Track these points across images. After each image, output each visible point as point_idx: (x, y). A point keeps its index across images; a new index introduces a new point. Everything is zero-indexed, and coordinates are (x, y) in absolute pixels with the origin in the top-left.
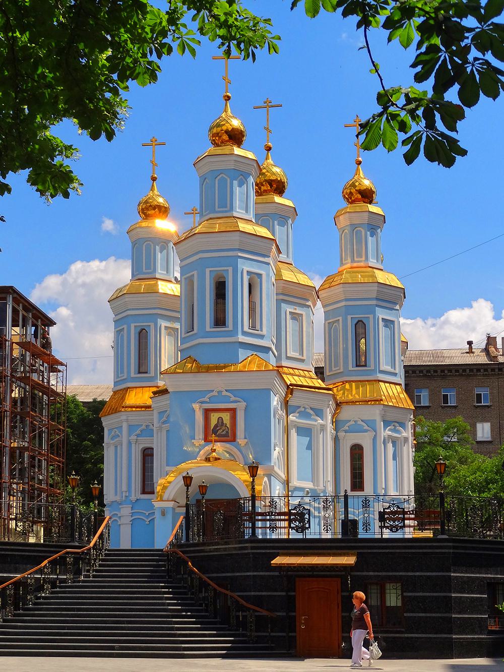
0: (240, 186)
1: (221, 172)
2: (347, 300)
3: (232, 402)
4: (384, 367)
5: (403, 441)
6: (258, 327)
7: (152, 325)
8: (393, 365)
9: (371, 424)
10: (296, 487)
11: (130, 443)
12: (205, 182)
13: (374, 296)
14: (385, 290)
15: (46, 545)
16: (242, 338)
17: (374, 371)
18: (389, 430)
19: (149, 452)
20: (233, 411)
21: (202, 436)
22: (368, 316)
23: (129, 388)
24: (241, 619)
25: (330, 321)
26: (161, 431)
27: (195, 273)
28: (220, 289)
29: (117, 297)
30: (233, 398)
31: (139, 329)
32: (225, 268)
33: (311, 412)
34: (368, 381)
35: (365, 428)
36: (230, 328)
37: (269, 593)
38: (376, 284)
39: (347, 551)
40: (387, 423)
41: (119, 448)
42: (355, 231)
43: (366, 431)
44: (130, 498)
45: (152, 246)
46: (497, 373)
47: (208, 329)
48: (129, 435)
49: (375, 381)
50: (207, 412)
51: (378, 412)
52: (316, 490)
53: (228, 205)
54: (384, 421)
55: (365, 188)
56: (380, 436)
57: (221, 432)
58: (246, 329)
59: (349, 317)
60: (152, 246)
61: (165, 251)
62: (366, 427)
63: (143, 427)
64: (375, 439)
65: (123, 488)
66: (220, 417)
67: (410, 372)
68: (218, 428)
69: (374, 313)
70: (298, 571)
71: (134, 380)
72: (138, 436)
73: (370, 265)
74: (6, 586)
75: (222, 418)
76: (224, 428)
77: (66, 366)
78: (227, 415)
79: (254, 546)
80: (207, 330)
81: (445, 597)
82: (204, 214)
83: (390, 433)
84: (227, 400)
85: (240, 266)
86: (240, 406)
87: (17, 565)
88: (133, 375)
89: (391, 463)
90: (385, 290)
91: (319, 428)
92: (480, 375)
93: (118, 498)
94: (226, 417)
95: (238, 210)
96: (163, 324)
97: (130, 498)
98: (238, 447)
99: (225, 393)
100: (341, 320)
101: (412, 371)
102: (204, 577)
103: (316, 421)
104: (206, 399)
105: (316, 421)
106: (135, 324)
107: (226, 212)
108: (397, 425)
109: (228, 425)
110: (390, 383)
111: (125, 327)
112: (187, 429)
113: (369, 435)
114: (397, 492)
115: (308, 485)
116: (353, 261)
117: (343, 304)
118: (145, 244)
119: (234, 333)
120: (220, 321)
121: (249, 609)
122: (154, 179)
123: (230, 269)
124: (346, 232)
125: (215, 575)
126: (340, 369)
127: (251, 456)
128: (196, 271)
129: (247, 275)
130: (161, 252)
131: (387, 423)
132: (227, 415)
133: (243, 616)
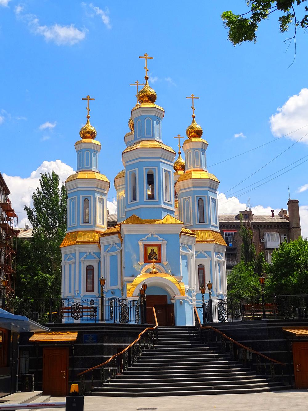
0: (157, 124)
1: (149, 116)
2: (194, 187)
4: (213, 224)
5: (223, 263)
6: (169, 200)
7: (92, 196)
8: (216, 223)
9: (209, 253)
11: (80, 263)
12: (138, 121)
13: (207, 185)
14: (213, 183)
15: (138, 325)
17: (208, 225)
18: (217, 257)
19: (90, 268)
20: (159, 246)
21: (143, 260)
22: (205, 196)
23: (78, 231)
24: (265, 367)
25: (184, 198)
26: (106, 256)
27: (137, 169)
30: (160, 239)
32: (135, 169)
33: (187, 247)
34: (205, 230)
35: (205, 256)
36: (157, 200)
37: (278, 352)
39: (298, 327)
40: (216, 253)
41: (73, 266)
42: (195, 152)
43: (206, 257)
44: (80, 294)
45: (199, 152)
46: (225, 227)
47: (145, 200)
48: (80, 258)
49: (209, 230)
50: (146, 246)
51: (212, 247)
53: (152, 134)
54: (215, 252)
56: (214, 260)
57: (152, 257)
59: (195, 196)
60: (199, 152)
61: (96, 156)
62: (206, 255)
63: (88, 254)
65: (76, 288)
66: (152, 249)
67: (222, 226)
68: (151, 255)
69: (207, 194)
70: (303, 338)
71: (82, 227)
72: (84, 258)
73: (203, 170)
75: (153, 249)
76: (154, 255)
77: (17, 218)
78: (156, 248)
79: (269, 324)
80: (145, 201)
82: (137, 138)
84: (156, 239)
85: (161, 167)
86: (164, 243)
88: (81, 224)
89: (218, 274)
90: (213, 183)
91: (191, 255)
92: (225, 228)
93: (72, 295)
94: (156, 249)
95: (156, 137)
96: (98, 196)
97: (80, 294)
98: (163, 265)
101: (230, 225)
102: (237, 342)
104: (145, 239)
105: (189, 251)
106: (82, 196)
107: (151, 137)
108: (220, 254)
111: (76, 197)
112: (135, 256)
113: (208, 259)
116: (194, 167)
117: (192, 189)
119: (159, 202)
121: (271, 361)
122: (194, 117)
123: (157, 168)
124: (190, 152)
125: (243, 341)
126: (191, 224)
127: (170, 272)
130: (94, 157)
131: (216, 253)
132: (156, 248)
133: (266, 365)
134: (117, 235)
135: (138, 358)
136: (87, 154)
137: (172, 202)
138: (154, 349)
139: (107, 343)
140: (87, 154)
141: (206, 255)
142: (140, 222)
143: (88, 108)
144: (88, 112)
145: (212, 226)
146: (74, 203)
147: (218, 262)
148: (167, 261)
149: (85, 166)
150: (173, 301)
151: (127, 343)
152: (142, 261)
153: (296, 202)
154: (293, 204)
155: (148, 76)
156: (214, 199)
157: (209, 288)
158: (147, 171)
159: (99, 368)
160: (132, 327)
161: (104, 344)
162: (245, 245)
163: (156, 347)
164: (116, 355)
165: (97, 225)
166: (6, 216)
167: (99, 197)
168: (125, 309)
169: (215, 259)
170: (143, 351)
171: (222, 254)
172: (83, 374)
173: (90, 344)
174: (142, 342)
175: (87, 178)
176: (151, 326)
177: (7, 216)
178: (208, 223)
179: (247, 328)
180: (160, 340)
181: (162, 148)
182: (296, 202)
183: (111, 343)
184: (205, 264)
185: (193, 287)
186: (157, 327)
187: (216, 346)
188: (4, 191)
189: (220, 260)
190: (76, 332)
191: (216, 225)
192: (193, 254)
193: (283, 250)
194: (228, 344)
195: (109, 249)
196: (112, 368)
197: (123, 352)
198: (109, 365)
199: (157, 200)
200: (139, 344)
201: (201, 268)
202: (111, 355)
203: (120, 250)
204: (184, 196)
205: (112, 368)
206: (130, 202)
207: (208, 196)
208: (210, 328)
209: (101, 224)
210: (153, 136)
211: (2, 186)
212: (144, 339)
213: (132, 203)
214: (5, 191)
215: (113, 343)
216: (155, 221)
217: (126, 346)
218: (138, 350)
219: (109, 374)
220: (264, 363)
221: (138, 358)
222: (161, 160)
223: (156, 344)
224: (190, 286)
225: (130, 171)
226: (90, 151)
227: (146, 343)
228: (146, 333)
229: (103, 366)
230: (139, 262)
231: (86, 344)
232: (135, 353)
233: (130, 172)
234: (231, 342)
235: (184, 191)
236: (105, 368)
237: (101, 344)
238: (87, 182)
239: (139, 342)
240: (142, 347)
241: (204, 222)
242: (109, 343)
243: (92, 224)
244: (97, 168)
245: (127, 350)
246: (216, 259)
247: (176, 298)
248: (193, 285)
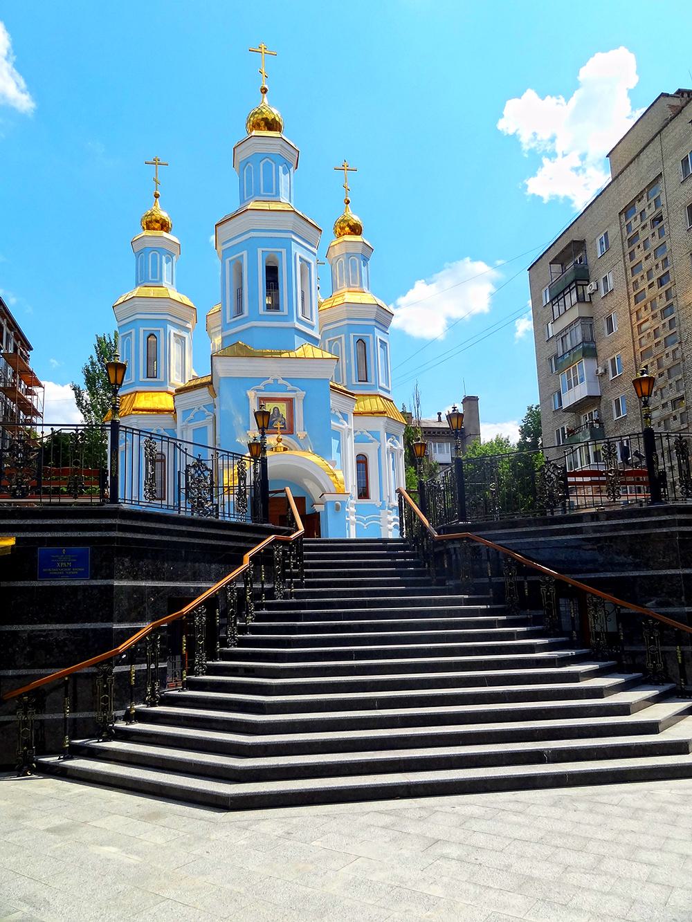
1: (267, 156)
2: (348, 319)
3: (289, 391)
4: (383, 384)
7: (162, 330)
9: (376, 435)
17: (374, 387)
18: (390, 442)
20: (290, 402)
23: (137, 392)
27: (245, 253)
28: (272, 273)
29: (124, 302)
30: (290, 387)
31: (148, 334)
33: (340, 416)
35: (370, 439)
38: (376, 306)
43: (371, 441)
47: (141, 379)
49: (376, 395)
50: (262, 400)
51: (382, 423)
59: (352, 335)
62: (371, 438)
74: (192, 611)
81: (105, 586)
82: (246, 199)
87: (197, 564)
88: (141, 379)
94: (283, 408)
96: (173, 330)
98: (297, 439)
99: (281, 381)
100: (343, 339)
104: (261, 387)
109: (285, 417)
110: (384, 398)
112: (240, 419)
116: (349, 286)
118: (150, 255)
120: (275, 306)
123: (284, 251)
128: (246, 251)
132: (283, 406)
133: (683, 653)
134: (206, 389)
135: (242, 630)
136: (154, 256)
137: (315, 322)
138: (294, 600)
139: (127, 578)
140: (154, 256)
141: (371, 438)
142: (250, 354)
145: (381, 388)
146: (129, 343)
147: (392, 452)
148: (304, 430)
149: (150, 279)
150: (318, 508)
151: (205, 580)
152: (255, 430)
153: (475, 399)
154: (471, 401)
155: (266, 86)
158: (266, 254)
159: (94, 670)
160: (225, 529)
161: (116, 583)
162: (410, 451)
163: (297, 595)
164: (164, 622)
165: (172, 381)
166: (24, 386)
167: (176, 332)
168: (199, 475)
169: (387, 445)
170: (258, 607)
171: (398, 438)
172: (27, 694)
173: (63, 583)
174: (256, 578)
175: (152, 296)
176: (285, 530)
177: (26, 387)
178: (373, 383)
179: (598, 535)
180: (309, 575)
181: (294, 211)
182: (475, 399)
183: (142, 580)
184: (367, 453)
185: (350, 490)
186: (300, 537)
187: (489, 591)
188: (19, 342)
189: (394, 447)
190: (10, 537)
191: (387, 388)
192: (350, 430)
193: (474, 453)
194: (535, 586)
195: (191, 417)
196: (144, 666)
197: (185, 610)
198: (133, 656)
199: (286, 313)
200: (246, 584)
201: (362, 461)
202: (142, 620)
203: (211, 417)
204: (331, 335)
205: (144, 666)
206: (231, 319)
207: (374, 335)
208: (468, 538)
209: (180, 380)
210: (278, 193)
211: (3, 317)
212: (261, 571)
213: (235, 319)
214: (21, 342)
215: (153, 580)
216: (280, 353)
217: (200, 591)
218: (241, 606)
219: (129, 690)
220: (676, 646)
221: (242, 630)
222: (294, 237)
223: (297, 585)
225: (230, 259)
226: (159, 253)
227: (268, 580)
228: (268, 551)
229: (111, 659)
230: (248, 432)
231: (46, 584)
232: (232, 613)
233: (230, 262)
234: (547, 578)
235: (332, 326)
236: (116, 669)
237: (105, 582)
238: (156, 303)
239: (244, 574)
240: (256, 595)
241: (366, 381)
242: (135, 578)
243: (162, 379)
244: (172, 284)
245: (200, 605)
246: (388, 444)
247: (327, 497)
248: (350, 487)
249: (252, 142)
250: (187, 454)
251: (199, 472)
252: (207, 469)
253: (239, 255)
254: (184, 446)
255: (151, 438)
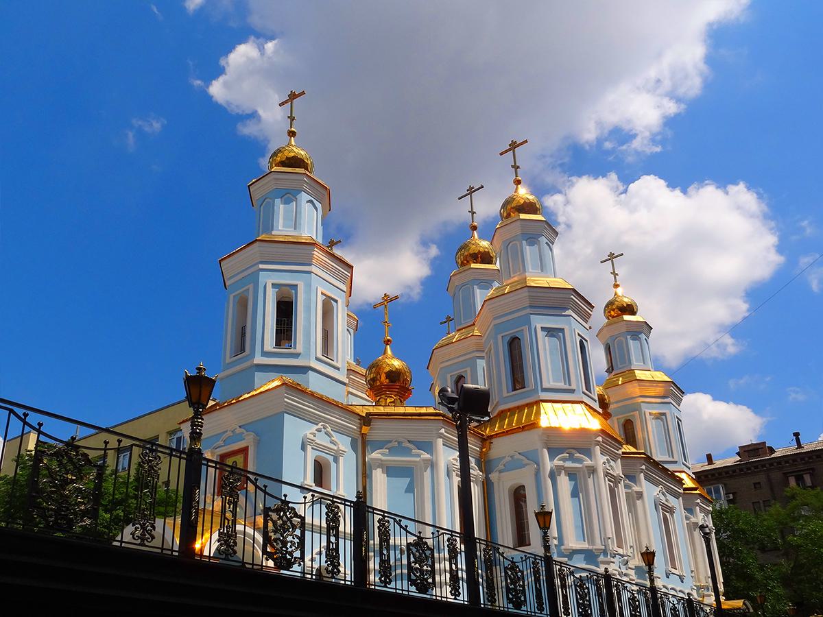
10: (573, 550)
14: (539, 294)
16: (259, 359)
22: (522, 328)
33: (242, 430)
43: (524, 466)
47: (505, 394)
52: (591, 550)
54: (549, 450)
55: (522, 202)
58: (319, 355)
59: (500, 337)
64: (537, 474)
83: (561, 463)
88: (505, 394)
90: (539, 294)
99: (239, 430)
103: (419, 456)
104: (221, 443)
105: (419, 456)
108: (573, 451)
114: (584, 541)
115: (585, 546)
128: (252, 285)
129: (272, 288)
143: (614, 272)
144: (615, 278)
156: (561, 329)
157: (542, 526)
207: (571, 326)
222: (261, 266)
224: (591, 540)
225: (234, 294)
233: (234, 296)
249: (272, 177)
250: (266, 493)
251: (285, 518)
252: (296, 515)
253: (244, 289)
254: (404, 522)
255: (384, 516)
